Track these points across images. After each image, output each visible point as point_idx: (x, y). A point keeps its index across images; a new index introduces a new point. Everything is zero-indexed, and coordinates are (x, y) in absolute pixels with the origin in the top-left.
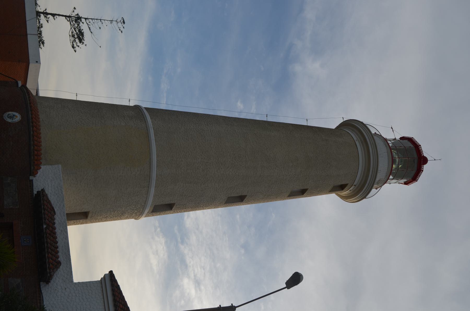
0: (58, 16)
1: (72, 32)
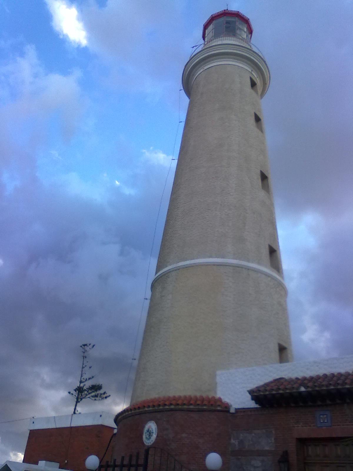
1: (93, 396)
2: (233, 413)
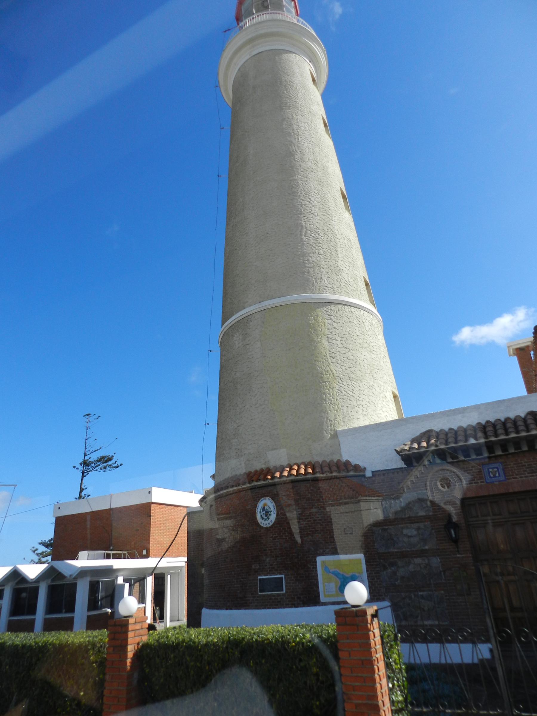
0: (83, 485)
1: (101, 469)
2: (370, 477)
